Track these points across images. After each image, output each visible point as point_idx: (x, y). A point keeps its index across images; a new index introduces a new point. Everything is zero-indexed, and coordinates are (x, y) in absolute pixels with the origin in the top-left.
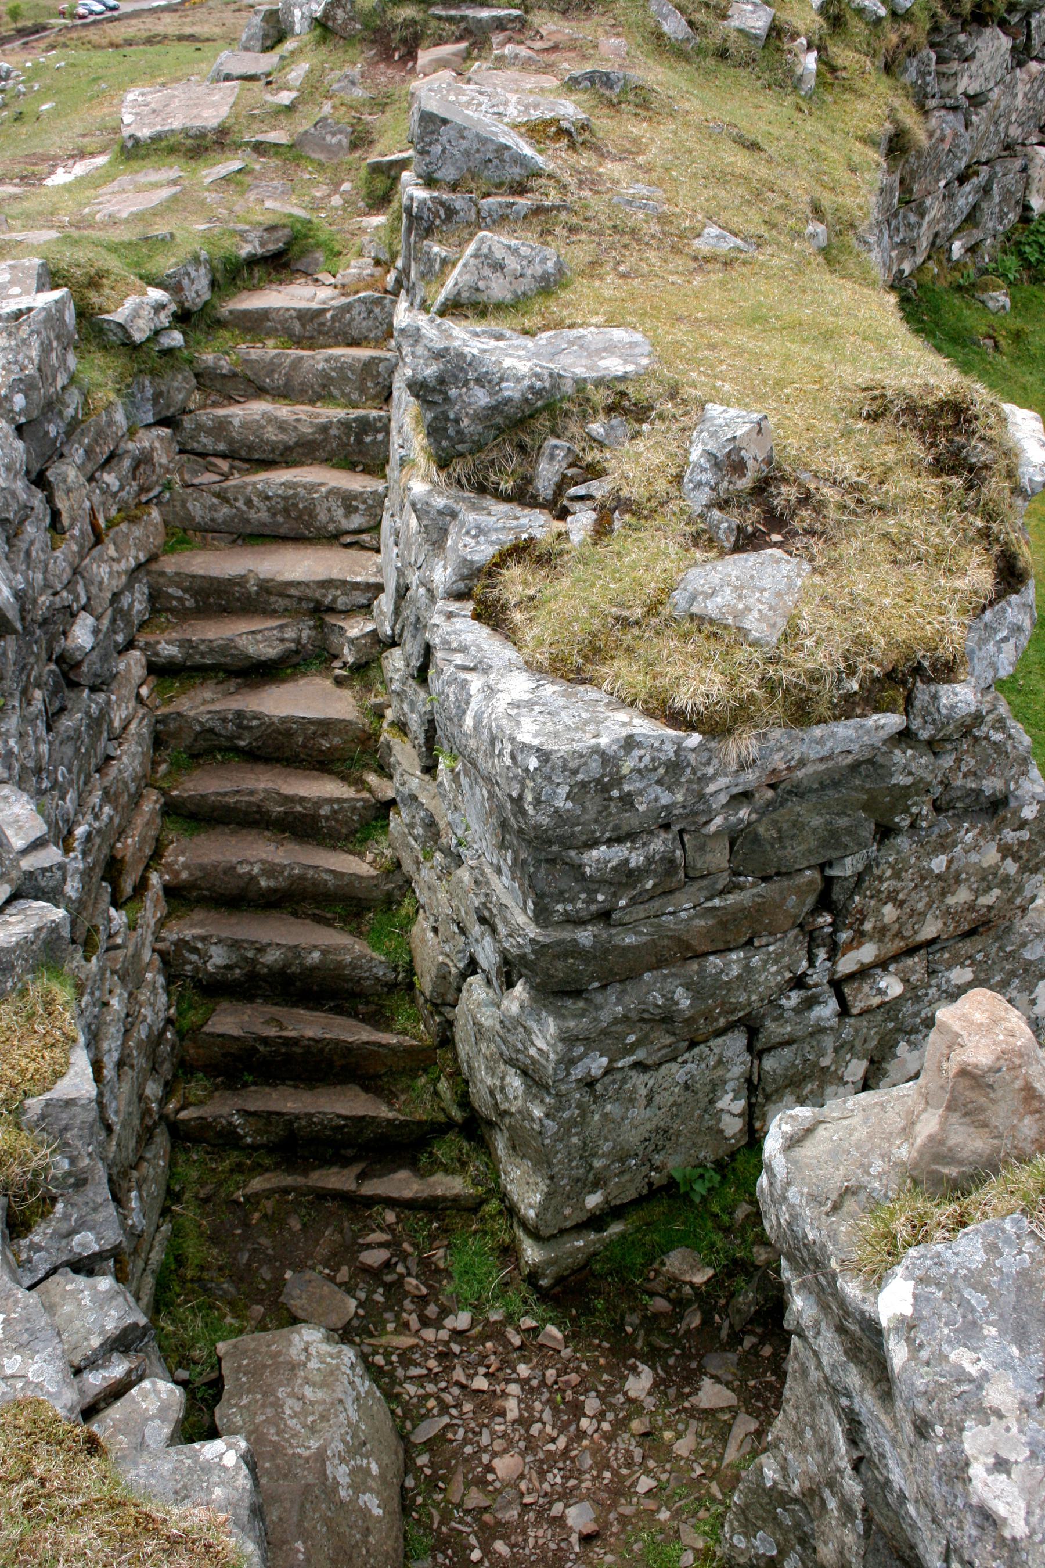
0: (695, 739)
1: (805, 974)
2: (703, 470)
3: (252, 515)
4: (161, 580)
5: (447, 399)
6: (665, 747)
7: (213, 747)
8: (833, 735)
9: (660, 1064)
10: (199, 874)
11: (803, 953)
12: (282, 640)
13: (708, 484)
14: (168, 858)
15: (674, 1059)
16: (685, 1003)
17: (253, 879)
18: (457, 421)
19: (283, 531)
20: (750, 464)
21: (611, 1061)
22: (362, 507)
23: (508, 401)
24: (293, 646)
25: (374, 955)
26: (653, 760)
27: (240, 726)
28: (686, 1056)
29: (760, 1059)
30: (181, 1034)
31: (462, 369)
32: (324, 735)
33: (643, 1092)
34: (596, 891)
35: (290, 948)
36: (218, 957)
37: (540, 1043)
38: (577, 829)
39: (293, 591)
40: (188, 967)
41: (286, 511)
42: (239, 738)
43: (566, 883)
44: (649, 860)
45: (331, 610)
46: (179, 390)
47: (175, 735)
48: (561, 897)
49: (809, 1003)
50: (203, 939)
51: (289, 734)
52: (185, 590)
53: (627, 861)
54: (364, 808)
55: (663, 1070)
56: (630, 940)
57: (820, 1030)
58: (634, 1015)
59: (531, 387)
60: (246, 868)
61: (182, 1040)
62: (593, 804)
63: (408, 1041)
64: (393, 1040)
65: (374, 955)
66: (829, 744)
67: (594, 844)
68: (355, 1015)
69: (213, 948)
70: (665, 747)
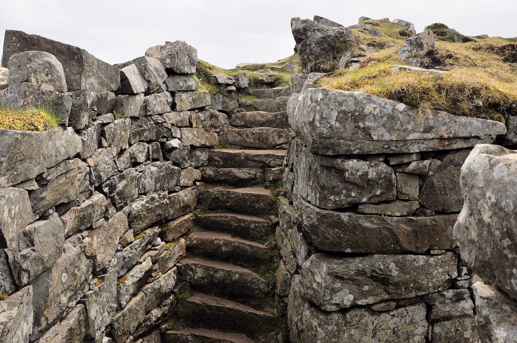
0: (401, 106)
1: (456, 280)
2: (405, 46)
3: (248, 140)
4: (213, 154)
5: (307, 37)
6: (387, 107)
7: (217, 205)
8: (471, 123)
9: (381, 312)
10: (200, 242)
11: (455, 267)
12: (249, 174)
13: (407, 50)
14: (191, 235)
15: (388, 312)
16: (395, 273)
17: (220, 246)
18: (310, 45)
19: (257, 146)
20: (425, 45)
21: (355, 299)
22: (284, 135)
23: (330, 36)
24: (253, 176)
25: (260, 278)
26: (381, 112)
27: (228, 197)
28: (394, 312)
29: (433, 326)
30: (177, 300)
31: (313, 26)
32: (258, 202)
33: (371, 327)
34: (351, 190)
35: (227, 271)
36: (200, 273)
37: (318, 279)
38: (342, 141)
39: (256, 159)
40: (188, 277)
41: (259, 138)
42: (227, 202)
43: (335, 182)
44: (379, 175)
45: (269, 166)
46: (232, 105)
47: (205, 200)
48: (333, 191)
49: (459, 298)
50: (195, 265)
51: (244, 200)
52: (220, 158)
53: (367, 173)
54: (267, 226)
55: (383, 316)
56: (367, 224)
57: (464, 316)
58: (368, 271)
59: (338, 32)
60: (218, 241)
61: (177, 303)
62: (350, 125)
63: (268, 314)
64: (262, 313)
65: (260, 278)
66: (469, 129)
67: (349, 156)
68: (249, 305)
69: (198, 269)
70: (387, 107)
